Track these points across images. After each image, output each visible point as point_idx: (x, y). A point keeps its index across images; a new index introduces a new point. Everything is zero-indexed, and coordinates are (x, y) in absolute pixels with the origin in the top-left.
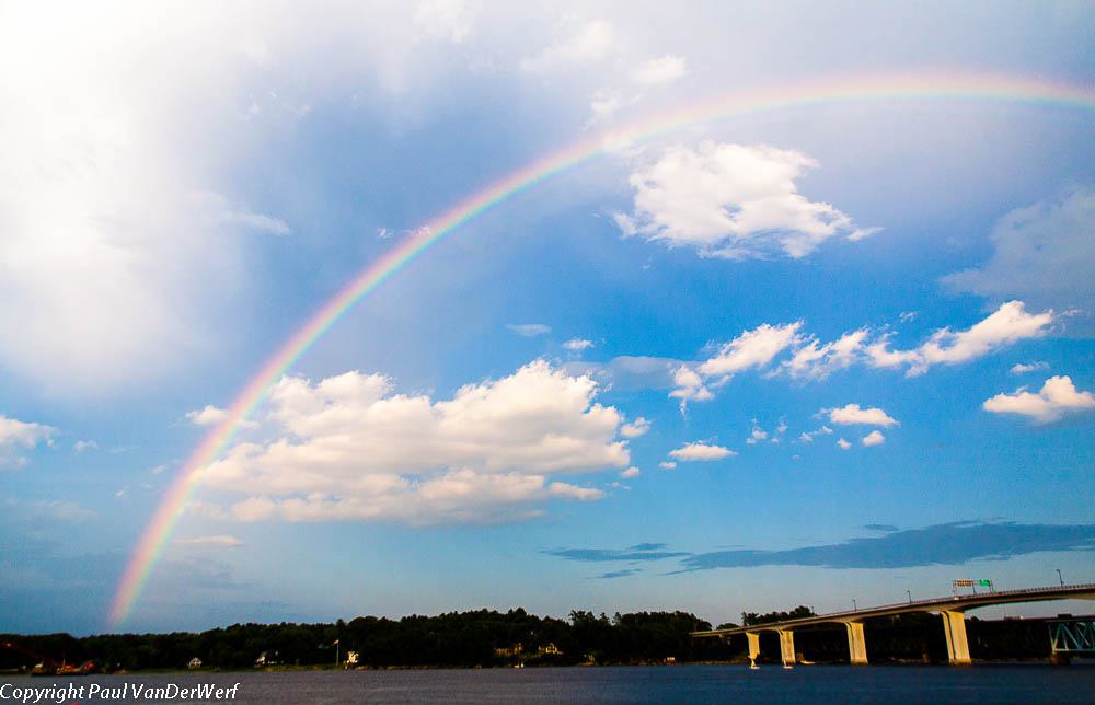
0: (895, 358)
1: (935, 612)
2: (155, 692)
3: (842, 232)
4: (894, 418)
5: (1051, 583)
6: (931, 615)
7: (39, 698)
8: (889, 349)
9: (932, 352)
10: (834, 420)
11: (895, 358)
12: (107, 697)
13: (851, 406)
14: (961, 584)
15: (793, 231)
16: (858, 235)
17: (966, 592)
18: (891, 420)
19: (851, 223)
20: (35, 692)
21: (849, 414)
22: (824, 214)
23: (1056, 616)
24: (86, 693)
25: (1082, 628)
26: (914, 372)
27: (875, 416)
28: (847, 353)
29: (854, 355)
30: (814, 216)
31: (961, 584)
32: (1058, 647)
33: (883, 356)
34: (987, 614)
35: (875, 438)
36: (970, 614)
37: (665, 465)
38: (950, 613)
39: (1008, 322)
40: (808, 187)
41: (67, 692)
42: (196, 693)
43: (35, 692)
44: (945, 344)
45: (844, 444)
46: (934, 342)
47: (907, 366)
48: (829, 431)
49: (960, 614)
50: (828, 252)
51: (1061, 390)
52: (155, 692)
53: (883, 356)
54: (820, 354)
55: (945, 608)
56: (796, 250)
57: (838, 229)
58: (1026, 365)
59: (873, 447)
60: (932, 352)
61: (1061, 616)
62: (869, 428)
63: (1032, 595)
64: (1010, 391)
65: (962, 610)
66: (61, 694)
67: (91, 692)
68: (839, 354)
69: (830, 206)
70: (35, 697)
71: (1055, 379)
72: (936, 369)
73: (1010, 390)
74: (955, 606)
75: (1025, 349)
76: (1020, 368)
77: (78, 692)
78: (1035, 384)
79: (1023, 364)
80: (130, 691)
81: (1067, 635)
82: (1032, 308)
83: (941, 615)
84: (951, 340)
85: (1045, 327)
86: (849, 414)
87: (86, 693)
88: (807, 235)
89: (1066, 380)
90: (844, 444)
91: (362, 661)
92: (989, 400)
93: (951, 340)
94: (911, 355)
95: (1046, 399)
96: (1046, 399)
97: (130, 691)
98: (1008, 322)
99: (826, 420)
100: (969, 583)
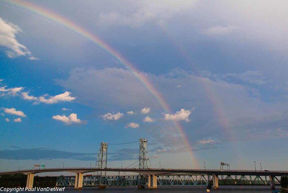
0: (31, 98)
1: (26, 174)
2: (43, 189)
3: (27, 56)
4: (26, 115)
5: (61, 167)
6: (24, 175)
7: (11, 190)
8: (30, 95)
9: (42, 99)
10: (5, 112)
11: (31, 98)
12: (44, 189)
13: (13, 108)
14: (36, 166)
15: (11, 49)
16: (32, 58)
17: (37, 168)
18: (25, 116)
19: (31, 54)
20: (10, 189)
21: (12, 111)
22: (23, 48)
23: (60, 176)
24: (24, 189)
25: (65, 179)
26: (35, 103)
27: (20, 113)
28: (15, 92)
29: (17, 94)
30: (19, 48)
31: (36, 166)
32: (58, 184)
33: (27, 96)
34: (41, 175)
35: (19, 120)
36: (36, 175)
37: (109, 116)
38: (30, 174)
39: (65, 96)
40: (18, 37)
41: (19, 189)
42: (54, 189)
43: (10, 189)
44: (47, 98)
45: (8, 120)
46: (44, 97)
47: (33, 101)
48: (3, 115)
49: (33, 175)
50: (21, 60)
51: (74, 117)
52: (43, 189)
53: (27, 96)
54: (6, 90)
55: (29, 173)
56: (10, 55)
57: (26, 54)
58: (67, 109)
59: (18, 123)
60: (42, 99)
61: (61, 176)
62: (17, 117)
63: (56, 170)
64: (61, 115)
65: (34, 173)
66: (17, 190)
67: (26, 189)
68: (12, 92)
69: (25, 47)
70: (10, 190)
71: (73, 114)
72: (43, 104)
73: (61, 115)
74: (32, 172)
75: (65, 104)
76: (64, 109)
77: (22, 189)
78: (68, 114)
79: (66, 108)
80: (36, 189)
81: (61, 181)
82: (71, 95)
83: (27, 175)
84: (49, 97)
85: (73, 100)
86: (12, 111)
87: (24, 189)
88: (16, 53)
89: (76, 115)
90: (8, 120)
91: (72, 179)
92: (54, 116)
93: (49, 97)
94: (36, 98)
95: (70, 118)
96: (70, 118)
97: (36, 189)
98: (65, 96)
99: (3, 111)
100: (39, 166)
